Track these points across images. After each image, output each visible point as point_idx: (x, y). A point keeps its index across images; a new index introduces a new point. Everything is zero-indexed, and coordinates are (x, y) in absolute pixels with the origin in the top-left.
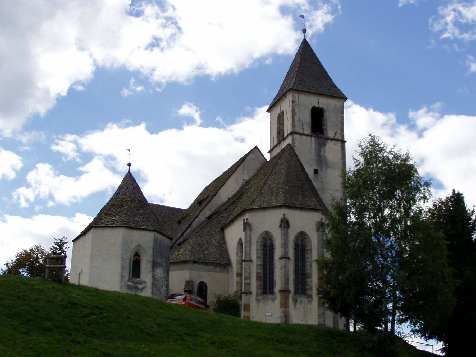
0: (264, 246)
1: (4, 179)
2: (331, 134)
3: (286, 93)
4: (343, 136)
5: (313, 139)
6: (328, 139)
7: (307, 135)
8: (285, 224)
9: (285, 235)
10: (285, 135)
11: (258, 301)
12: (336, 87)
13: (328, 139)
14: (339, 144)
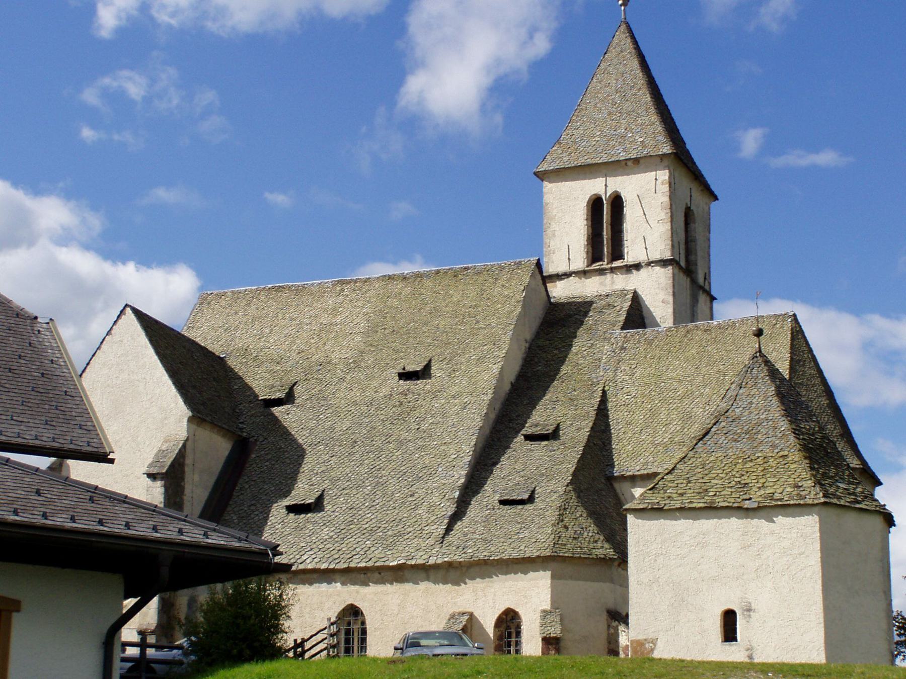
10: (633, 252)
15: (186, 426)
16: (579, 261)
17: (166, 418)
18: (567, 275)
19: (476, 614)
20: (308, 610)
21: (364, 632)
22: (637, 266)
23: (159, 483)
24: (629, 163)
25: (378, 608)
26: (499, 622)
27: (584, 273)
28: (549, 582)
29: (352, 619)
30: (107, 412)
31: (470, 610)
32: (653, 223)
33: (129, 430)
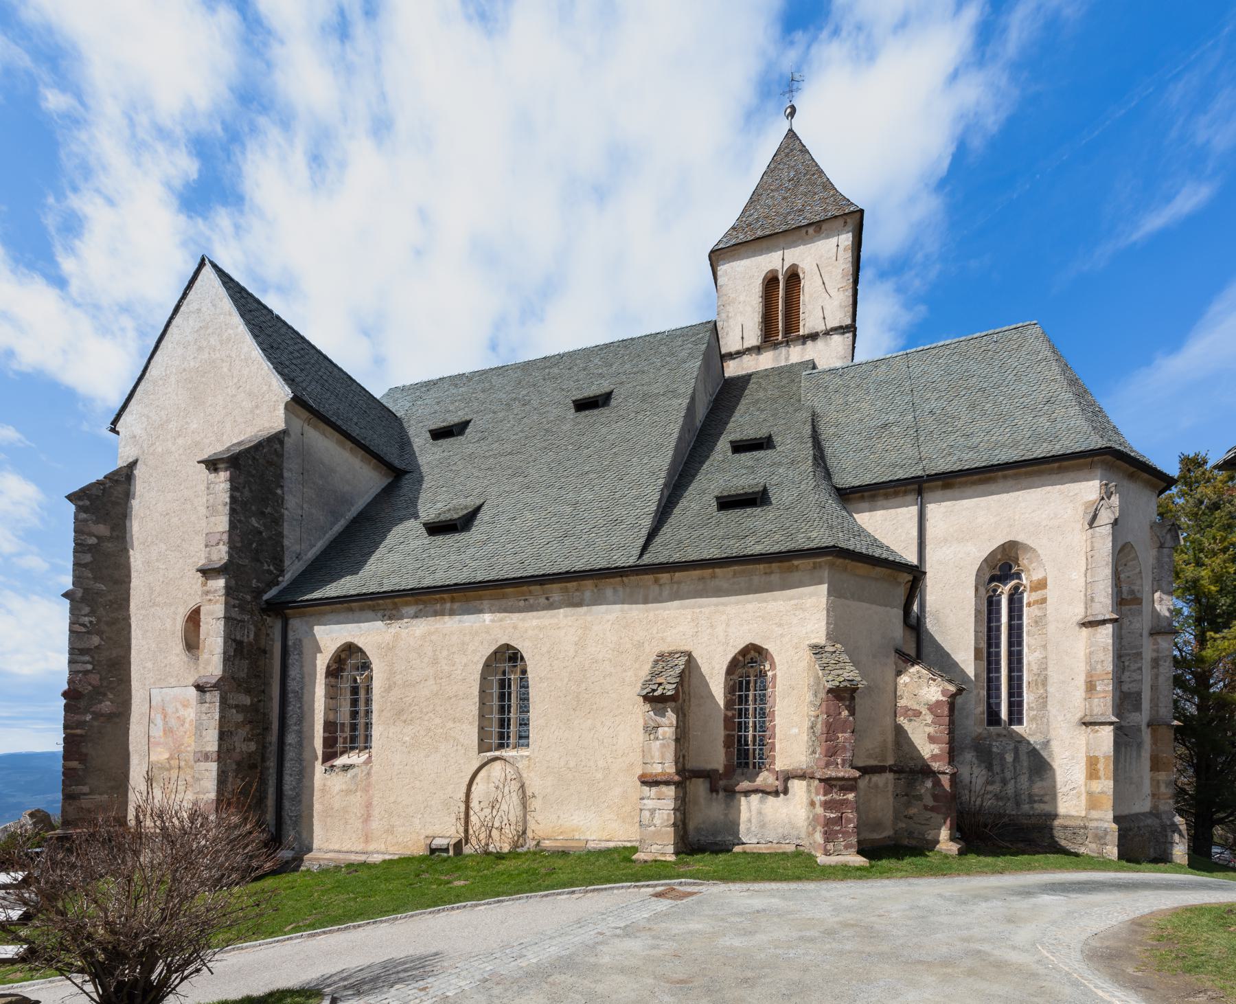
10: (810, 321)
15: (283, 416)
16: (753, 339)
17: (257, 407)
18: (739, 354)
19: (694, 654)
20: (445, 653)
21: (524, 685)
22: (814, 337)
23: (224, 476)
24: (811, 230)
25: (544, 649)
26: (733, 666)
27: (758, 350)
28: (824, 600)
29: (507, 665)
30: (183, 406)
31: (686, 648)
32: (833, 292)
33: (212, 426)
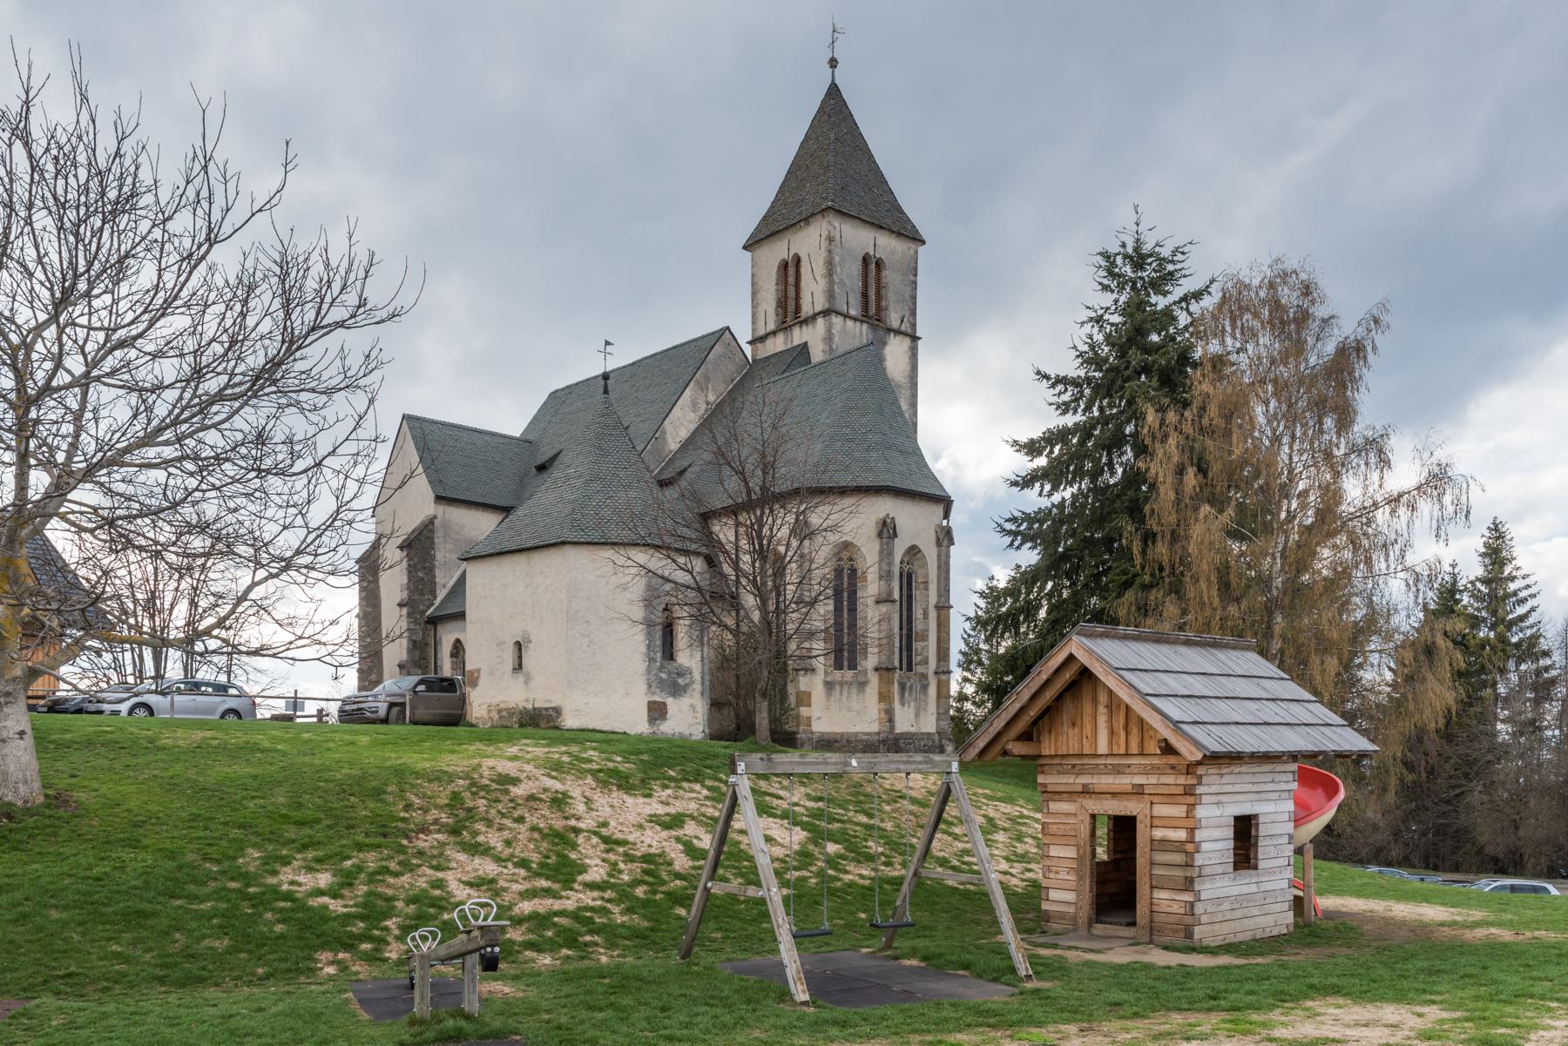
0: (839, 572)
1: (7, 812)
2: (894, 320)
3: (813, 215)
4: (914, 325)
5: (865, 326)
6: (890, 330)
7: (855, 319)
8: (887, 530)
9: (886, 553)
11: (829, 686)
12: (903, 212)
13: (890, 330)
14: (907, 342)
